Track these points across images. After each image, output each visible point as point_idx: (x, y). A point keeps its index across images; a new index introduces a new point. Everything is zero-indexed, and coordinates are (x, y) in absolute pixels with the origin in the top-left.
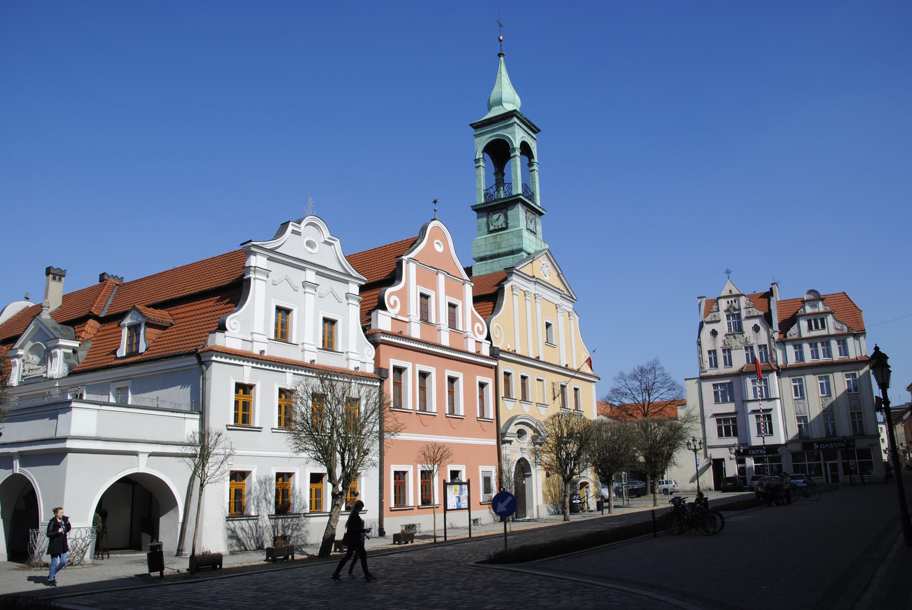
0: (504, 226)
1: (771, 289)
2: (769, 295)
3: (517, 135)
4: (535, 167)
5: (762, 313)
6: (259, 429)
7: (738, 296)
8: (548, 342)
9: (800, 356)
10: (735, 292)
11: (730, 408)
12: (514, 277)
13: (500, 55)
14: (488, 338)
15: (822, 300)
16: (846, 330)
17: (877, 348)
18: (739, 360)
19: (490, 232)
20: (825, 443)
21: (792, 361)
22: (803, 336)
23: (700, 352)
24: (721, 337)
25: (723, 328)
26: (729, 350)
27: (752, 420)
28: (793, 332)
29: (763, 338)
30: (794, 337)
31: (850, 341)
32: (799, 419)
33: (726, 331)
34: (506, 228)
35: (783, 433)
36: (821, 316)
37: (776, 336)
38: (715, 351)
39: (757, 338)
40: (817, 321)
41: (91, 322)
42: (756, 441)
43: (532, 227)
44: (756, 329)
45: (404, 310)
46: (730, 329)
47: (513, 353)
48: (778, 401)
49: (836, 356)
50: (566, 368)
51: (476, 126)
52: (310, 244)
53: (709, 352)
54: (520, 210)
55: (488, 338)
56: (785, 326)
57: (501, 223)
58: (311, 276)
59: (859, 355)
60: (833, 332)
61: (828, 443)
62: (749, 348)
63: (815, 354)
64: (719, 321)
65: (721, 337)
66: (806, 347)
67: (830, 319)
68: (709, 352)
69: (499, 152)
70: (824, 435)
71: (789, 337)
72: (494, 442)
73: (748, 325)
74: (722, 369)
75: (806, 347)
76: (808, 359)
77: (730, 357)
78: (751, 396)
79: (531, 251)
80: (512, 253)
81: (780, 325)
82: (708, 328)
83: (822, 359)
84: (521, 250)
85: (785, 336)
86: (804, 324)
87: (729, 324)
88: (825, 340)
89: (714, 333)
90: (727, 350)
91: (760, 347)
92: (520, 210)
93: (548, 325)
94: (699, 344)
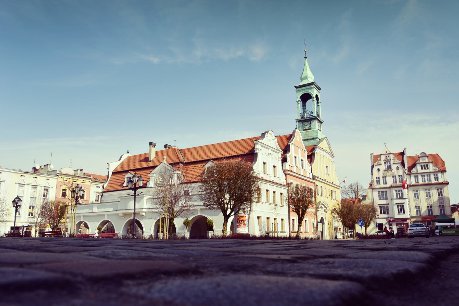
0: (310, 128)
1: (403, 151)
2: (403, 154)
3: (314, 92)
4: (320, 104)
5: (400, 162)
6: (262, 203)
7: (390, 154)
8: (327, 174)
9: (417, 180)
10: (388, 152)
11: (384, 202)
12: (317, 149)
13: (305, 58)
14: (312, 172)
15: (427, 157)
16: (438, 170)
18: (390, 182)
19: (304, 130)
21: (413, 182)
22: (419, 172)
23: (373, 178)
24: (381, 172)
25: (382, 167)
26: (385, 177)
27: (396, 208)
28: (414, 170)
29: (401, 172)
30: (414, 172)
31: (440, 175)
32: (416, 207)
34: (311, 129)
35: (410, 213)
36: (427, 164)
37: (407, 172)
38: (379, 178)
40: (425, 166)
41: (181, 164)
42: (397, 216)
43: (319, 129)
44: (398, 168)
45: (291, 163)
46: (386, 168)
48: (407, 199)
49: (433, 181)
50: (332, 183)
51: (296, 87)
52: (269, 140)
53: (377, 178)
54: (316, 121)
55: (312, 172)
56: (410, 169)
57: (308, 127)
58: (270, 151)
59: (443, 181)
60: (432, 171)
62: (394, 176)
63: (424, 180)
64: (381, 165)
66: (420, 178)
67: (431, 165)
68: (377, 178)
69: (305, 98)
70: (427, 215)
71: (412, 172)
72: (315, 211)
73: (394, 167)
74: (382, 185)
75: (420, 178)
76: (421, 182)
77: (386, 180)
78: (395, 197)
79: (320, 138)
80: (313, 139)
81: (408, 168)
82: (376, 168)
83: (427, 182)
84: (317, 138)
85: (411, 172)
86: (419, 167)
87: (385, 166)
88: (429, 174)
89: (379, 170)
90: (384, 177)
91: (399, 176)
92: (316, 121)
93: (327, 167)
94: (372, 174)
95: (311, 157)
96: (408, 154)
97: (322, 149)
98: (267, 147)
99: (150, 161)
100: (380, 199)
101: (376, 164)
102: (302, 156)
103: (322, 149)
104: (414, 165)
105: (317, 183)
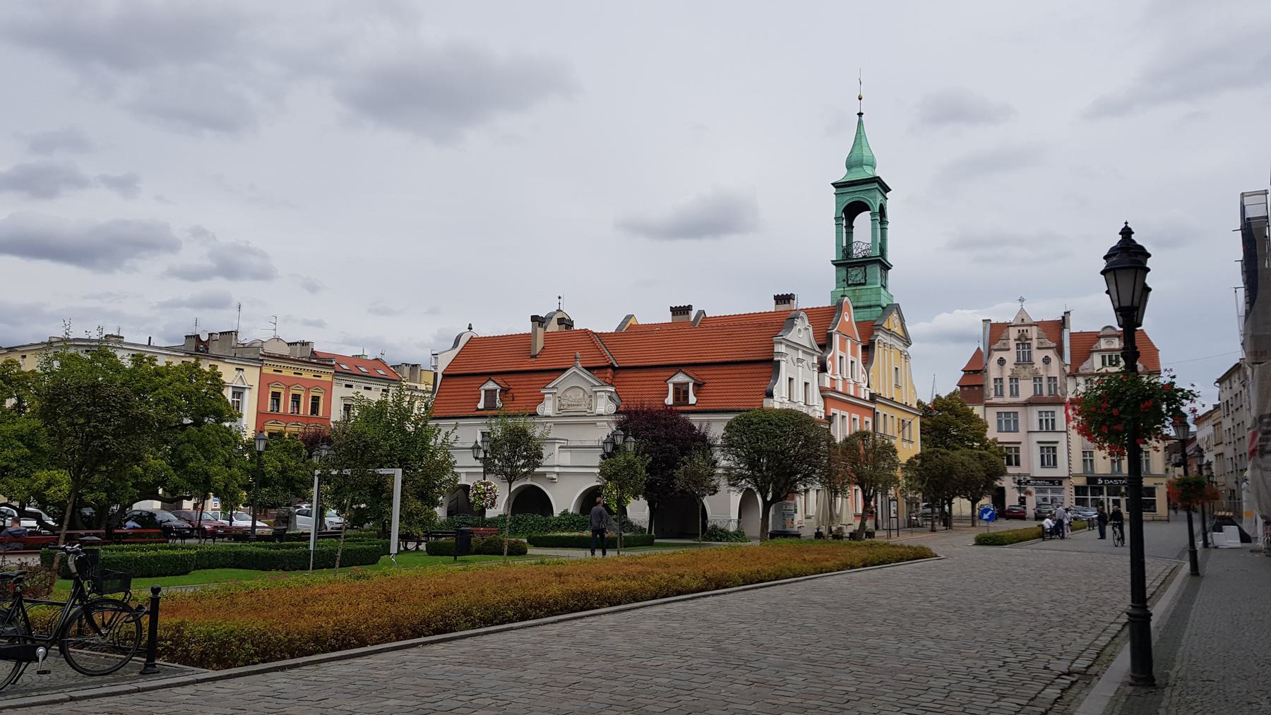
2: (1062, 323)
8: (897, 386)
17: (1127, 232)
19: (849, 285)
20: (1110, 479)
25: (1011, 357)
33: (1015, 360)
38: (1001, 379)
39: (1047, 370)
44: (1047, 360)
47: (892, 400)
50: (905, 405)
54: (878, 268)
57: (859, 278)
58: (801, 355)
61: (1113, 479)
62: (1037, 378)
65: (1010, 365)
73: (1038, 356)
74: (1007, 398)
85: (1077, 370)
95: (868, 349)
96: (1075, 326)
97: (889, 332)
98: (795, 346)
99: (535, 356)
100: (1000, 431)
101: (995, 347)
102: (854, 353)
103: (889, 332)
104: (1087, 355)
105: (878, 409)
